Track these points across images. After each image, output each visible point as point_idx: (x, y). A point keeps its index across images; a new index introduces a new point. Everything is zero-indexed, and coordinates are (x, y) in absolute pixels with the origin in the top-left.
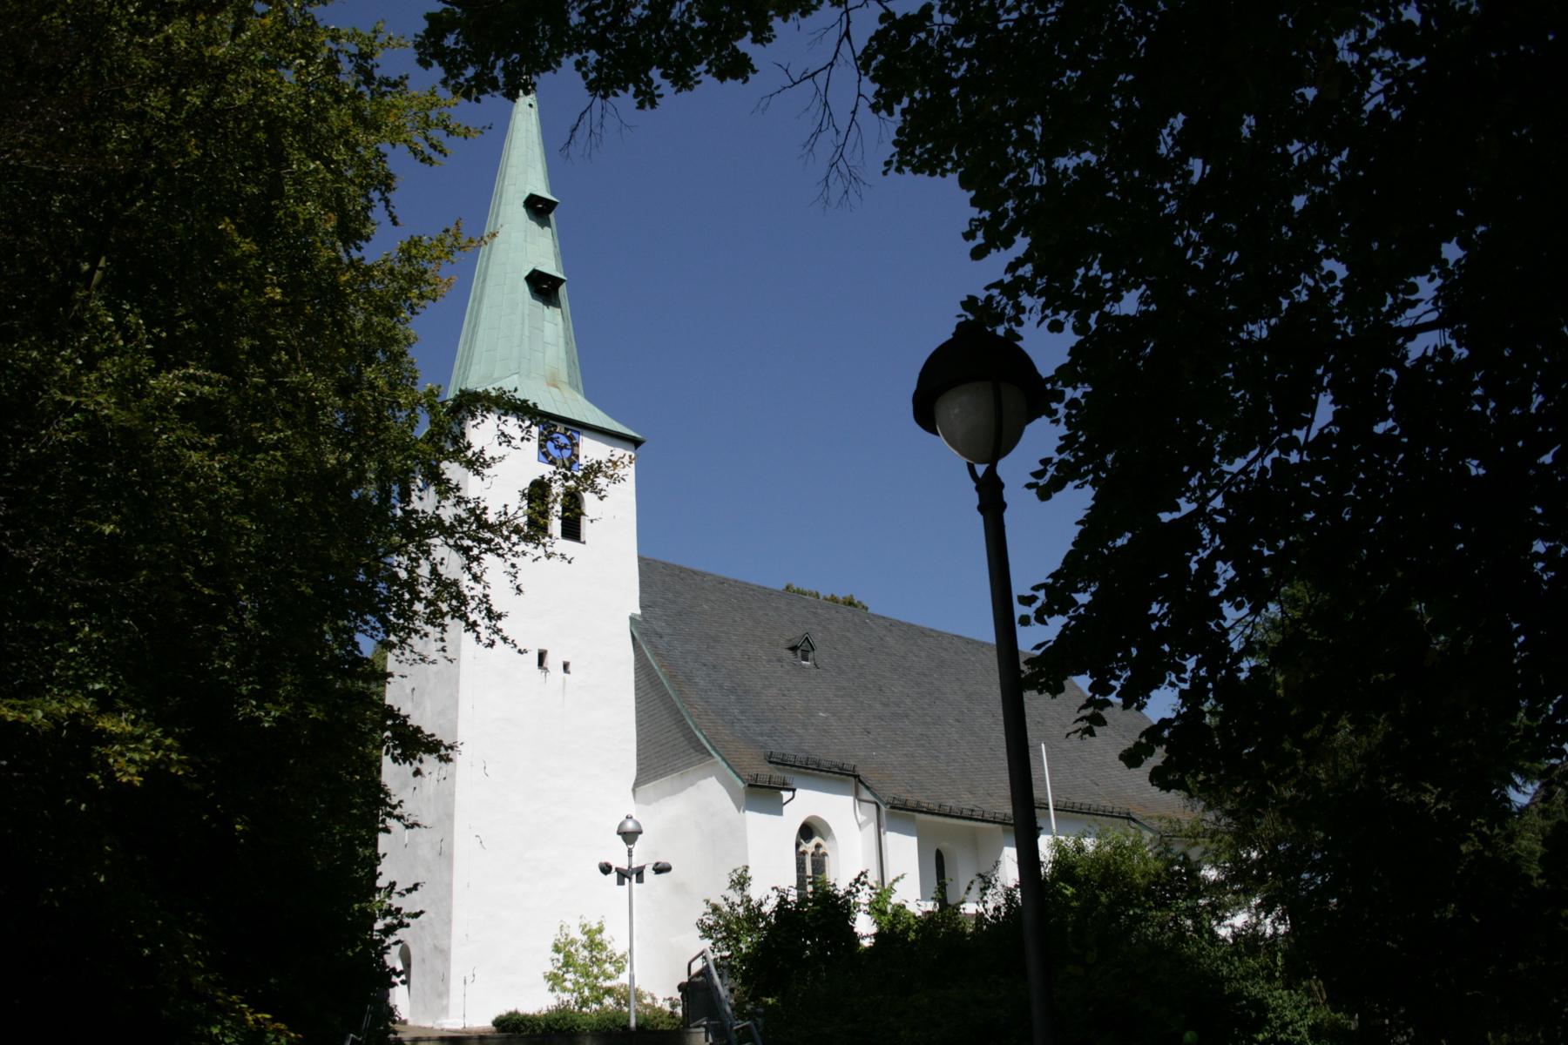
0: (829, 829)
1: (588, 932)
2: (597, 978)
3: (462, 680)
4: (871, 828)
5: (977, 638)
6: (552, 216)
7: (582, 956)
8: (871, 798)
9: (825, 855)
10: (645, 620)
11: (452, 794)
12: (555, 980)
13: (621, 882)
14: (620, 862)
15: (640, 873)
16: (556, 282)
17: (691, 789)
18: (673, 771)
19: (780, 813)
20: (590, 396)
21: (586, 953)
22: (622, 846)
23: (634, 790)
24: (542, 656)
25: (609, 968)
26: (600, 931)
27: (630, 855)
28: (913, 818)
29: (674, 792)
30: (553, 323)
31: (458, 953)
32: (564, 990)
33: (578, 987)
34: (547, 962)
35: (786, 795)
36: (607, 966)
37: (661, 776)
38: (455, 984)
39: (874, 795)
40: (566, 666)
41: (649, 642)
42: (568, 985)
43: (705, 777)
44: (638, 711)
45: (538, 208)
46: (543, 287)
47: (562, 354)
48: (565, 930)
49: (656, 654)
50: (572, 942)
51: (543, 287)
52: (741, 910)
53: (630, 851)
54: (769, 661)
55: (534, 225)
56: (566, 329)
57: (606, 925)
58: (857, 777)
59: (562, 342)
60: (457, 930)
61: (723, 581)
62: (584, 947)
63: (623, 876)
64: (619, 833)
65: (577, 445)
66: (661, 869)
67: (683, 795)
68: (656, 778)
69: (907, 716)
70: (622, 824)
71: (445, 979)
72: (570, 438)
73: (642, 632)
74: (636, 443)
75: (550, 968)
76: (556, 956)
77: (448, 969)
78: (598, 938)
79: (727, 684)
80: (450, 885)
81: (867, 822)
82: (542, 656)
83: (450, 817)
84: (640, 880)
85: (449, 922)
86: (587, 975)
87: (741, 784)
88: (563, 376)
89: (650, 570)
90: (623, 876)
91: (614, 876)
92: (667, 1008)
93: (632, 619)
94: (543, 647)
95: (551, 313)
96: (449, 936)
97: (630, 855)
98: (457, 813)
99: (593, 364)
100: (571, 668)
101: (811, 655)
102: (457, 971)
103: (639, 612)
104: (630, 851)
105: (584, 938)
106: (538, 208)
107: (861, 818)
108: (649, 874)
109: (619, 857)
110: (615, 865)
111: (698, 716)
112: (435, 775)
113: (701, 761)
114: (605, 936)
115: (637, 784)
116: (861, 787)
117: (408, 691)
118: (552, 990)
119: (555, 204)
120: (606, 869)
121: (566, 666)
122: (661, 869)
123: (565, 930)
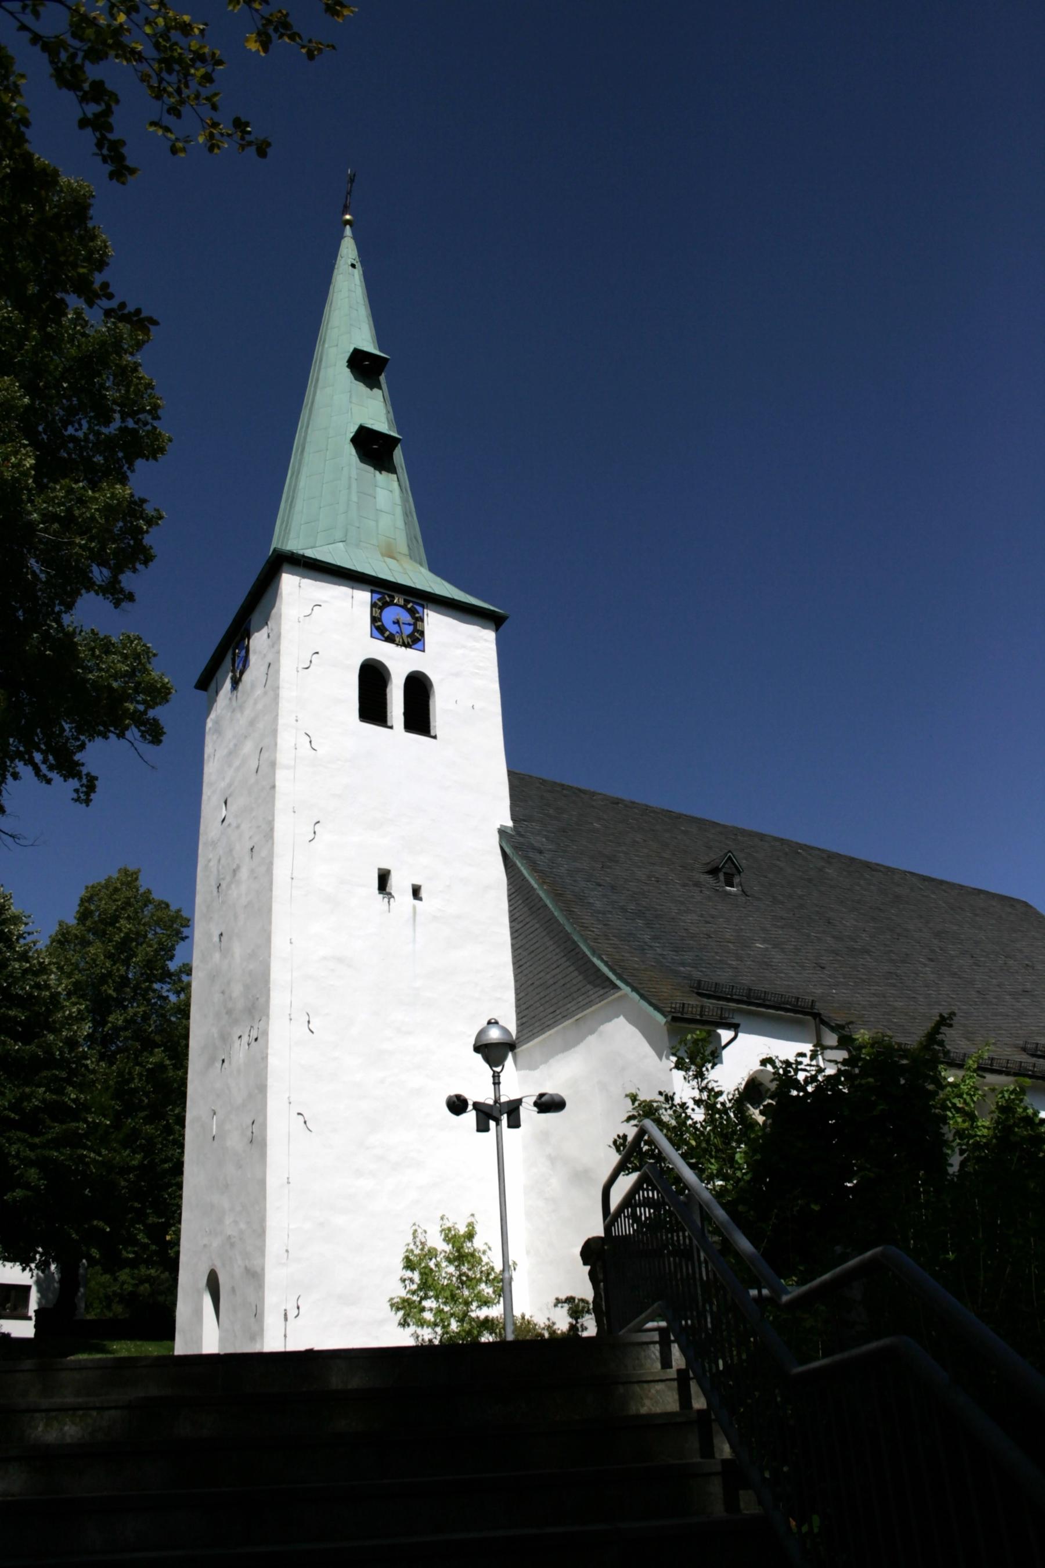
1: (450, 1236)
2: (467, 1303)
3: (276, 907)
5: (934, 876)
7: (449, 1269)
10: (519, 834)
11: (265, 1058)
14: (480, 1091)
15: (513, 1110)
16: (389, 442)
17: (591, 1039)
20: (435, 567)
21: (451, 1269)
22: (485, 1071)
24: (383, 879)
25: (487, 1290)
26: (470, 1236)
27: (496, 1083)
29: (568, 1046)
30: (387, 493)
31: (274, 1275)
32: (422, 1323)
33: (441, 1319)
34: (395, 1283)
37: (549, 1027)
40: (416, 892)
41: (526, 858)
42: (428, 1316)
43: (610, 1020)
44: (515, 948)
45: (364, 367)
46: (372, 448)
47: (400, 523)
49: (533, 867)
50: (432, 1253)
51: (372, 448)
52: (698, 1115)
53: (496, 1077)
54: (684, 885)
55: (361, 387)
56: (404, 501)
57: (477, 1228)
58: (816, 1016)
59: (399, 511)
60: (274, 1245)
61: (617, 802)
62: (450, 1261)
63: (486, 1116)
64: (477, 1049)
65: (422, 620)
66: (549, 1104)
67: (581, 1048)
69: (868, 952)
70: (482, 1033)
72: (412, 612)
73: (515, 847)
75: (401, 1292)
76: (408, 1274)
77: (262, 1299)
78: (468, 1247)
79: (632, 907)
80: (262, 1183)
82: (383, 879)
83: (262, 1088)
85: (261, 1233)
86: (453, 1298)
87: (661, 1019)
88: (402, 546)
89: (521, 786)
90: (486, 1116)
91: (470, 1117)
92: (562, 1322)
93: (502, 832)
94: (385, 866)
95: (383, 478)
96: (262, 1250)
97: (496, 1083)
98: (271, 1082)
99: (437, 530)
100: (423, 893)
101: (736, 880)
103: (510, 824)
104: (496, 1077)
105: (448, 1248)
108: (528, 1112)
109: (478, 1087)
110: (472, 1097)
111: (595, 940)
112: (245, 1039)
113: (602, 998)
114: (478, 1243)
116: (824, 1028)
118: (404, 1324)
119: (385, 361)
120: (457, 1105)
121: (416, 892)
122: (549, 1104)
123: (421, 1237)
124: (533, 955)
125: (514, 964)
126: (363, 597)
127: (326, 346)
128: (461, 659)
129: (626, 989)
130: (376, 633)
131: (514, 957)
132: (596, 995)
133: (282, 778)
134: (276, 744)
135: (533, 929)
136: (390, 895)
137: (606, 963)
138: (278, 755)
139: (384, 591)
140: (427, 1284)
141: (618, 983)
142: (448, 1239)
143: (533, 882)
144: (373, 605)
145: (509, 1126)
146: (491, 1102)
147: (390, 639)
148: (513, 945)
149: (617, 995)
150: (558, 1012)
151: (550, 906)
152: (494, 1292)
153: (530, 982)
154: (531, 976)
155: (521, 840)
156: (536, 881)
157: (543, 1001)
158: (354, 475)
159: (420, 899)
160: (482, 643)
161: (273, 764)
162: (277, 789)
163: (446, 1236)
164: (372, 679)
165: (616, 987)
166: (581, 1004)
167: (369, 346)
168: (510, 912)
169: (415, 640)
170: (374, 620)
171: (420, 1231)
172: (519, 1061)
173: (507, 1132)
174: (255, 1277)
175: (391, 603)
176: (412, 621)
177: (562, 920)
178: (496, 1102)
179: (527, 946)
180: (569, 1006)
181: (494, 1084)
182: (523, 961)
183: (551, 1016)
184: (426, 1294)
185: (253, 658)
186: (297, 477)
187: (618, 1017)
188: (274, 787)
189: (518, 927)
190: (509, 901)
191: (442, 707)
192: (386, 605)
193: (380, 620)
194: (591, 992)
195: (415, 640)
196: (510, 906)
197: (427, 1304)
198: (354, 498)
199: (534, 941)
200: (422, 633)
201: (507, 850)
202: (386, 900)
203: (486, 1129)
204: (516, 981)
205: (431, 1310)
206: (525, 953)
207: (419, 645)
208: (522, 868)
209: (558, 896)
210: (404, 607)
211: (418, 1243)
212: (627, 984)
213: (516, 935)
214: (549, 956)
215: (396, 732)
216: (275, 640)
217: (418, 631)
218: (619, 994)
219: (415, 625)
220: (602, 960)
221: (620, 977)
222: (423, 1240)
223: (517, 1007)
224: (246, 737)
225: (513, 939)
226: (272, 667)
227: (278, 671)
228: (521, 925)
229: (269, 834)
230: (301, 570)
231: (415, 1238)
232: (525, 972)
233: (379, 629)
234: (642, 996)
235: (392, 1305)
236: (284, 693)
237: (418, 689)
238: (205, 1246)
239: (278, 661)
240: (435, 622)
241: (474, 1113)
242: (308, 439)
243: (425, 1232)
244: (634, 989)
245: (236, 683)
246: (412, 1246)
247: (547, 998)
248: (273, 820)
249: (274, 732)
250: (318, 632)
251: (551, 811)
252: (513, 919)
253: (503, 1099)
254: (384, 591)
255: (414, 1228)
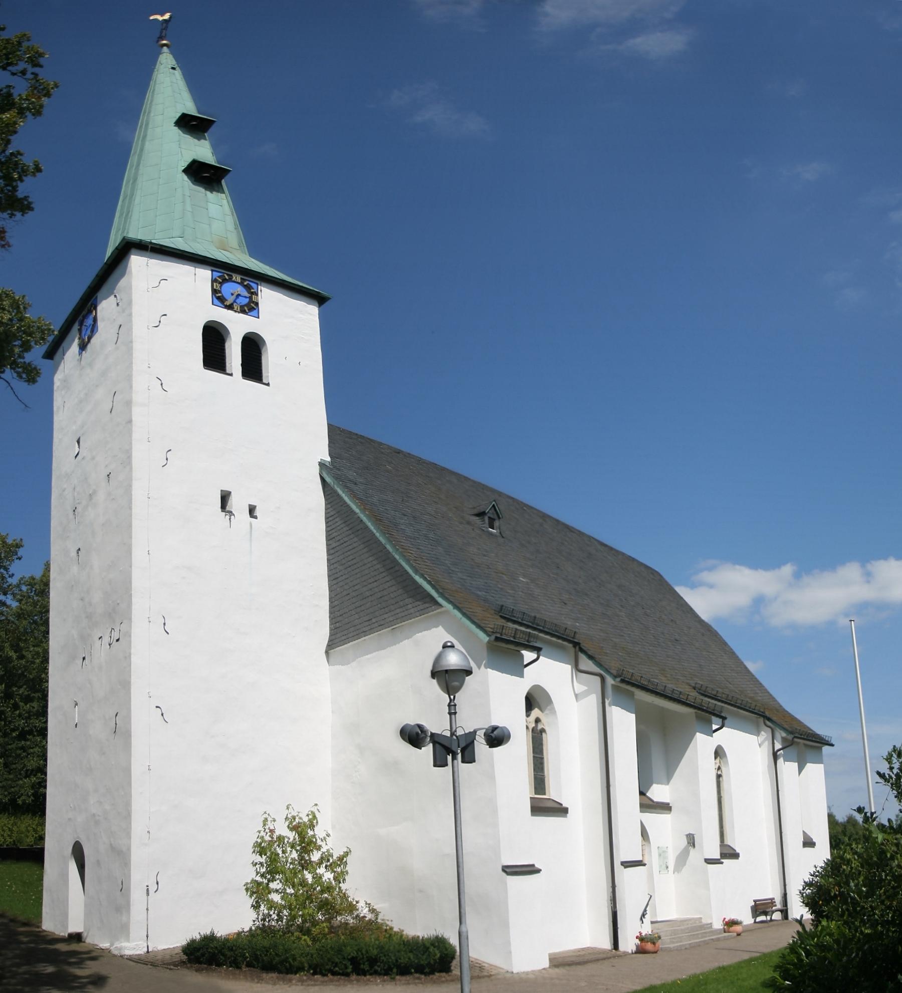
0: (549, 701)
4: (593, 700)
6: (223, 182)
8: (597, 669)
9: (543, 731)
11: (128, 657)
12: (258, 891)
13: (439, 762)
14: (438, 725)
18: (381, 626)
19: (521, 675)
23: (327, 652)
24: (225, 498)
26: (312, 826)
27: (452, 713)
28: (632, 695)
31: (139, 855)
35: (528, 656)
36: (321, 870)
37: (365, 633)
38: (137, 895)
39: (599, 664)
40: (252, 510)
46: (199, 173)
48: (270, 825)
51: (199, 173)
60: (138, 826)
68: (357, 636)
70: (438, 659)
71: (124, 888)
72: (248, 288)
73: (333, 477)
74: (319, 299)
76: (258, 859)
80: (127, 771)
81: (585, 694)
82: (225, 498)
83: (126, 685)
84: (469, 757)
87: (485, 638)
91: (428, 750)
93: (322, 465)
95: (212, 196)
96: (129, 835)
97: (452, 713)
100: (257, 513)
102: (139, 878)
106: (186, 123)
107: (580, 688)
108: (481, 746)
112: (106, 639)
113: (422, 612)
115: (331, 645)
117: (73, 554)
121: (252, 510)
123: (270, 825)
124: (349, 569)
125: (329, 576)
126: (205, 275)
127: (152, 115)
128: (290, 326)
129: (448, 606)
130: (216, 301)
131: (329, 570)
132: (416, 609)
133: (137, 414)
134: (131, 387)
135: (350, 547)
136: (231, 513)
137: (429, 583)
138: (134, 395)
139: (224, 271)
140: (273, 868)
141: (440, 600)
142: (292, 828)
143: (354, 507)
144: (214, 281)
145: (463, 762)
146: (448, 734)
147: (230, 307)
148: (328, 560)
149: (439, 610)
150: (374, 620)
151: (372, 528)
152: (335, 879)
153: (345, 593)
154: (346, 587)
155: (339, 473)
156: (358, 507)
157: (358, 610)
158: (187, 193)
159: (256, 517)
160: (308, 314)
161: (129, 404)
162: (134, 423)
163: (291, 823)
164: (213, 340)
165: (441, 606)
166: (400, 615)
167: (190, 108)
168: (327, 531)
169: (251, 308)
170: (214, 291)
171: (269, 819)
172: (331, 659)
173: (464, 768)
174: (122, 856)
175: (230, 280)
176: (247, 295)
177: (382, 540)
178: (452, 734)
179: (344, 561)
180: (386, 616)
181: (450, 714)
182: (339, 574)
183: (367, 623)
184: (274, 877)
185: (100, 324)
186: (130, 203)
187: (437, 626)
188: (130, 421)
189: (334, 545)
190: (327, 523)
191: (272, 360)
192: (225, 281)
193: (220, 292)
194: (410, 606)
195: (251, 308)
196: (327, 527)
197: (274, 885)
198: (189, 208)
199: (351, 557)
200: (257, 304)
201: (328, 479)
202: (228, 517)
203: (445, 765)
204: (331, 591)
205: (277, 891)
206: (341, 568)
207: (254, 313)
208: (343, 495)
209: (377, 519)
210: (241, 284)
211: (267, 831)
212: (450, 602)
213: (332, 551)
214: (367, 572)
215: (234, 380)
216: (126, 307)
217: (253, 302)
218: (443, 609)
219: (251, 298)
220: (425, 579)
221: (442, 595)
222: (272, 828)
223: (331, 613)
224: (97, 386)
225: (329, 554)
226: (123, 329)
227: (130, 329)
228: (338, 544)
229: (127, 461)
230: (148, 253)
231: (264, 825)
232: (341, 584)
233: (219, 298)
234: (464, 614)
235: (247, 890)
236: (137, 346)
237: (253, 347)
238: (70, 819)
239: (131, 321)
240: (267, 296)
241: (430, 747)
242: (140, 172)
243: (274, 821)
244: (456, 607)
245: (83, 347)
246: (262, 834)
247: (363, 608)
248: (131, 448)
249: (129, 378)
250: (163, 304)
251: (354, 453)
252: (329, 538)
253: (460, 732)
254: (224, 271)
255: (266, 816)
